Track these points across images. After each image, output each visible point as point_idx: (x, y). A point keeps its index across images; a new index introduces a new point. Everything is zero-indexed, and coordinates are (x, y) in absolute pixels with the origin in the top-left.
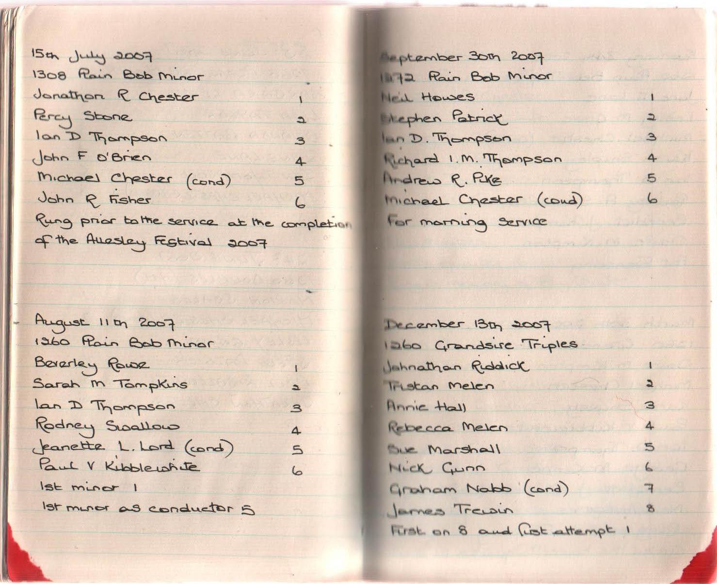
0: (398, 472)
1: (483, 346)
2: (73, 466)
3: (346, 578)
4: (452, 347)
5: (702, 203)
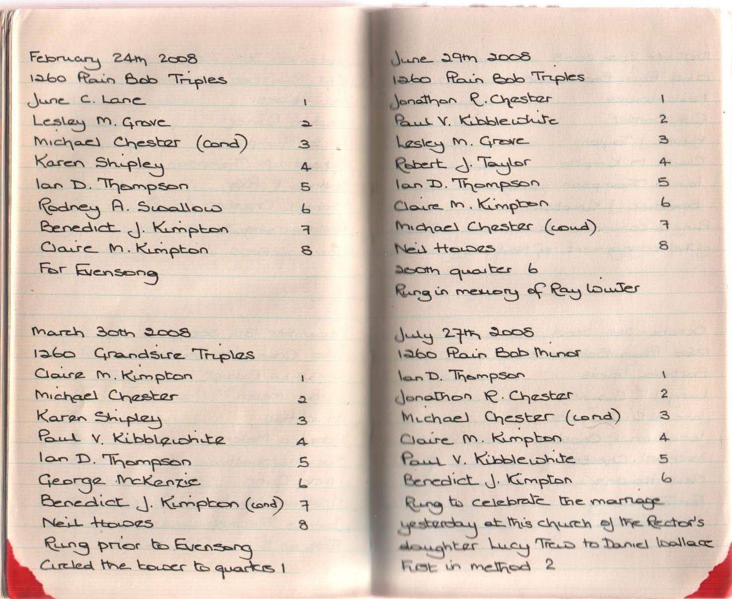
2: (78, 524)
3: (355, 593)
5: (717, 165)
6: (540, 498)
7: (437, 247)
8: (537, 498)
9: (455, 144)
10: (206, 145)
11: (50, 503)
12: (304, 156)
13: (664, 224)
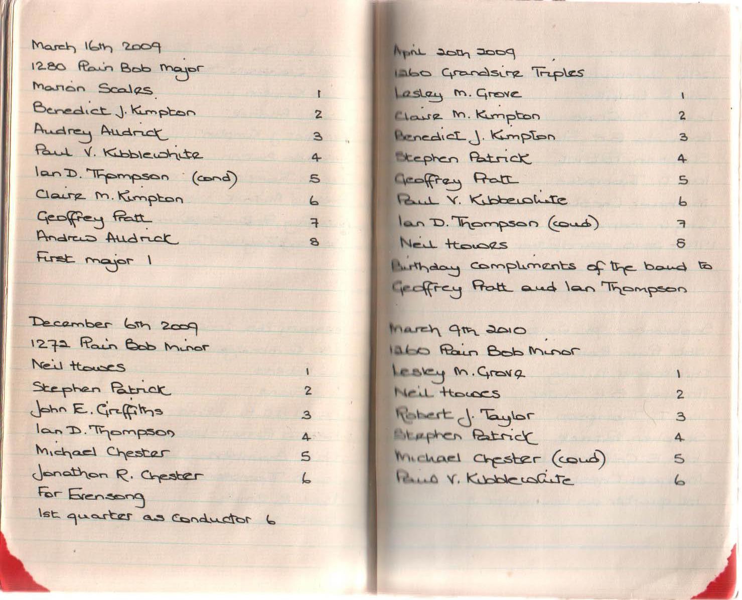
0: (409, 247)
1: (485, 73)
4: (458, 73)
9: (455, 116)
11: (42, 109)
12: (315, 147)
13: (313, 223)
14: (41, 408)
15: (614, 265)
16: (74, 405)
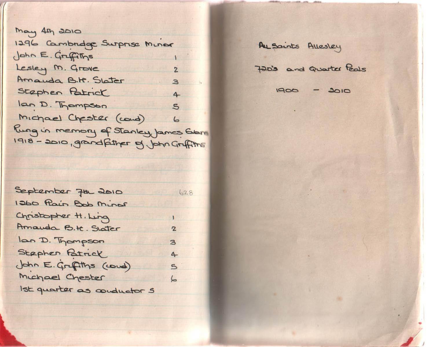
6: (116, 79)
7: (109, 133)
8: (115, 79)
10: (18, 216)
14: (23, 264)
15: (81, 55)
16: (45, 263)
